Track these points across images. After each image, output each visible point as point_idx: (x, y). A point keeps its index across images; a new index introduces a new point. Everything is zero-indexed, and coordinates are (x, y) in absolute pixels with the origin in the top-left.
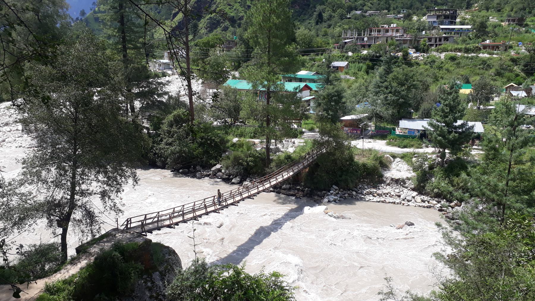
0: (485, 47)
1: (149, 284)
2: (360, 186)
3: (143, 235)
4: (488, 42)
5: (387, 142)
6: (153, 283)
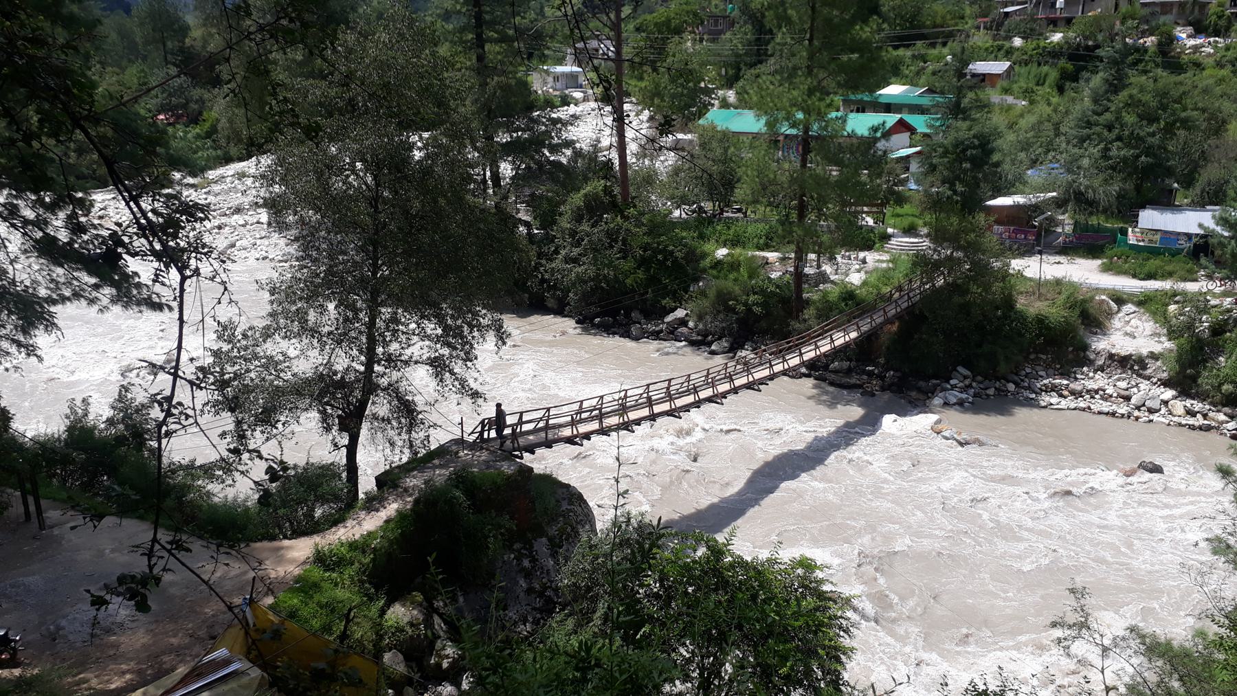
2: (1028, 370)
5: (1103, 264)
6: (534, 560)
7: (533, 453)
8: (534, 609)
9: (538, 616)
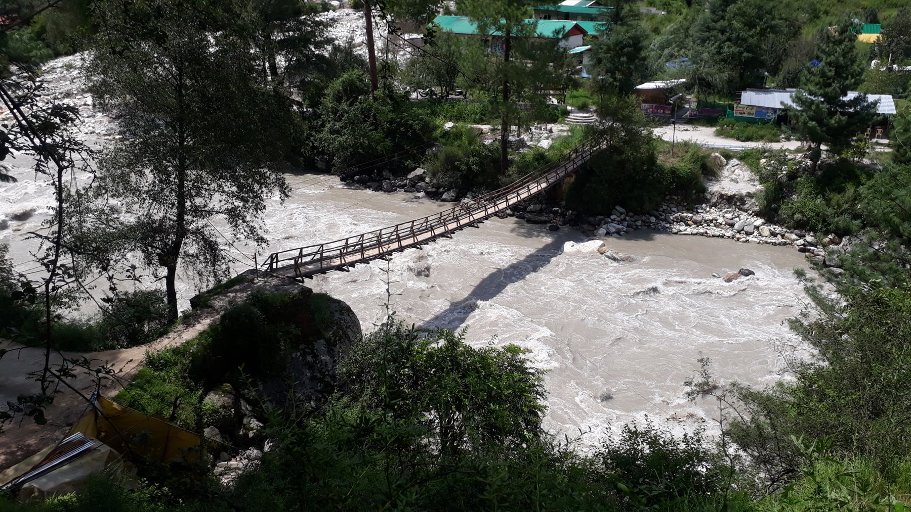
2: (665, 207)
5: (717, 130)
8: (317, 391)
9: (320, 396)
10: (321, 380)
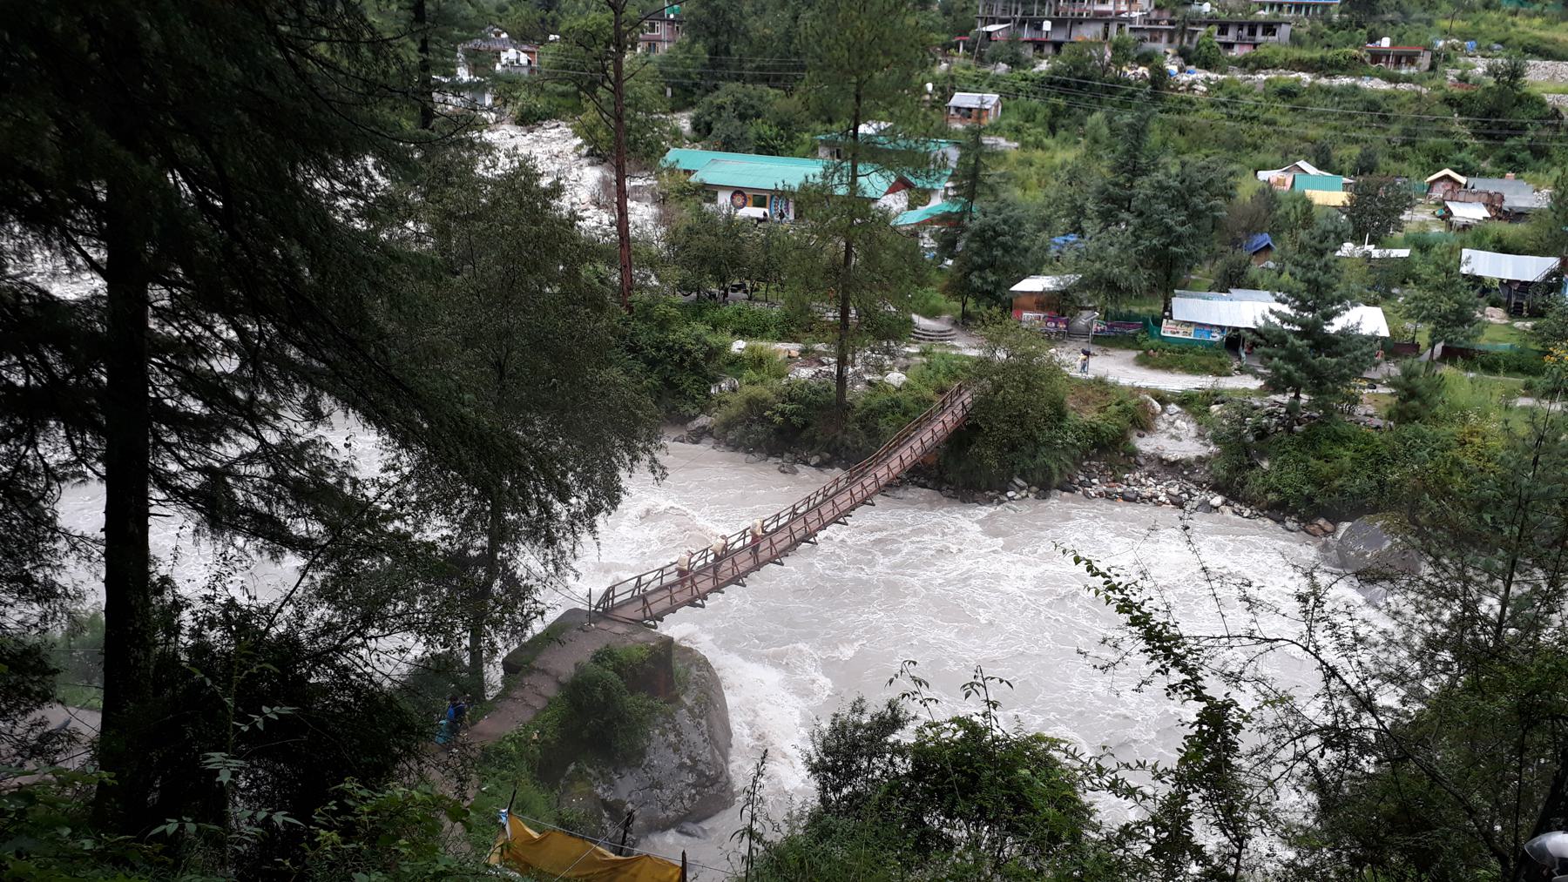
0: (1377, 56)
1: (672, 738)
2: (1082, 478)
3: (646, 625)
4: (1385, 42)
5: (1138, 356)
6: (679, 734)
7: (662, 620)
8: (688, 785)
9: (693, 791)
10: (692, 769)
